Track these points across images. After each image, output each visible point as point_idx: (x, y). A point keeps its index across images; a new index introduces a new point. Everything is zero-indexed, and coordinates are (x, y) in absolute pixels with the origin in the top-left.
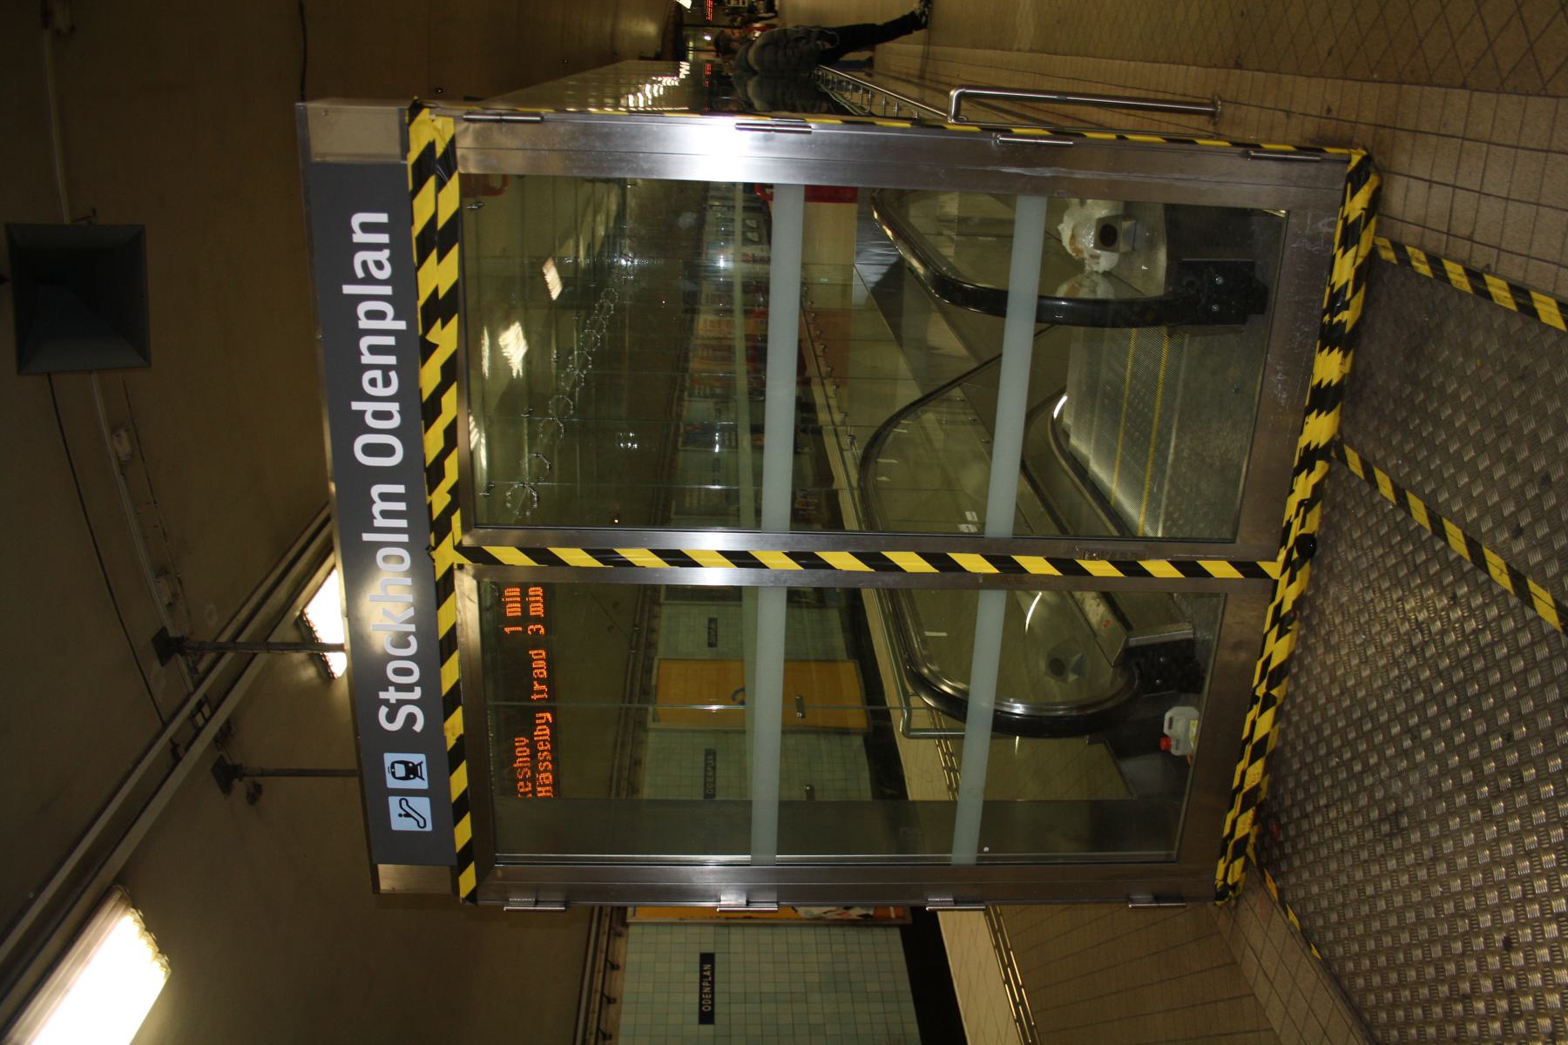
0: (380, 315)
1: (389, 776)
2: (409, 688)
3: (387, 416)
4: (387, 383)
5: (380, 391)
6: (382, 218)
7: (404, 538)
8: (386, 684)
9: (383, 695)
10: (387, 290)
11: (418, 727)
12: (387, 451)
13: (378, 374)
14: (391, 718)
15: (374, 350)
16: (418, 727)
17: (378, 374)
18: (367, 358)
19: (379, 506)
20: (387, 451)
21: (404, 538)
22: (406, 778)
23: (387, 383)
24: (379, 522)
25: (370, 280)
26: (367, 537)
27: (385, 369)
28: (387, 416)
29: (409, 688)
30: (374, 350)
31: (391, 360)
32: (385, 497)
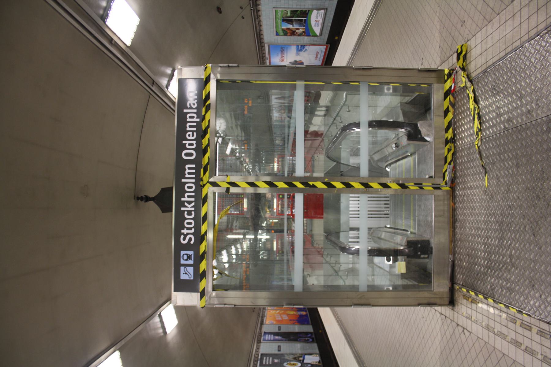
0: (193, 117)
1: (181, 259)
2: (190, 229)
3: (192, 145)
4: (193, 136)
5: (191, 138)
6: (194, 166)
7: (194, 181)
8: (184, 227)
9: (182, 231)
10: (195, 111)
11: (192, 242)
12: (191, 155)
13: (191, 133)
14: (184, 239)
15: (190, 127)
16: (192, 242)
17: (191, 133)
18: (188, 129)
19: (188, 171)
20: (191, 155)
21: (194, 181)
22: (187, 260)
23: (193, 136)
24: (187, 176)
25: (191, 108)
26: (183, 180)
27: (193, 132)
28: (192, 145)
29: (190, 229)
30: (190, 127)
31: (195, 129)
32: (189, 168)
